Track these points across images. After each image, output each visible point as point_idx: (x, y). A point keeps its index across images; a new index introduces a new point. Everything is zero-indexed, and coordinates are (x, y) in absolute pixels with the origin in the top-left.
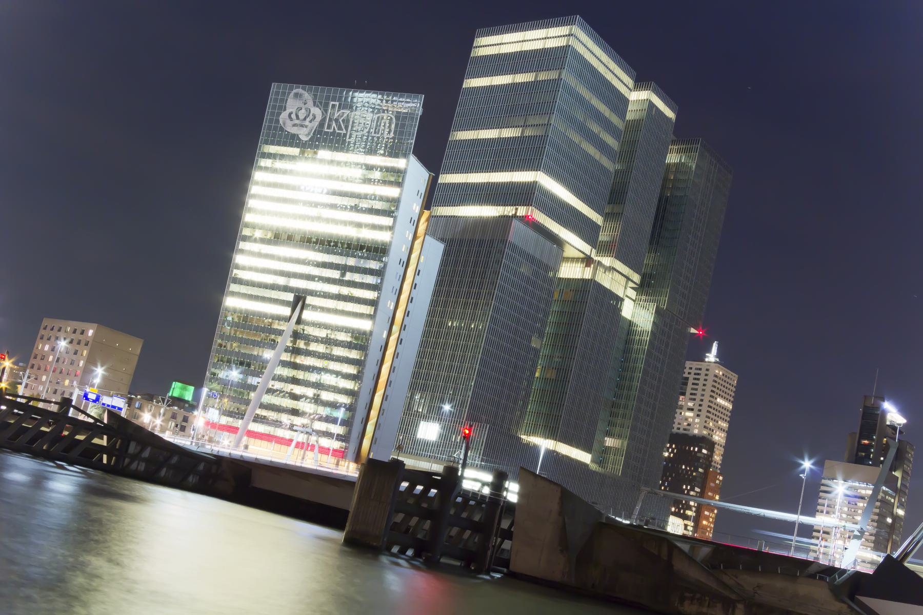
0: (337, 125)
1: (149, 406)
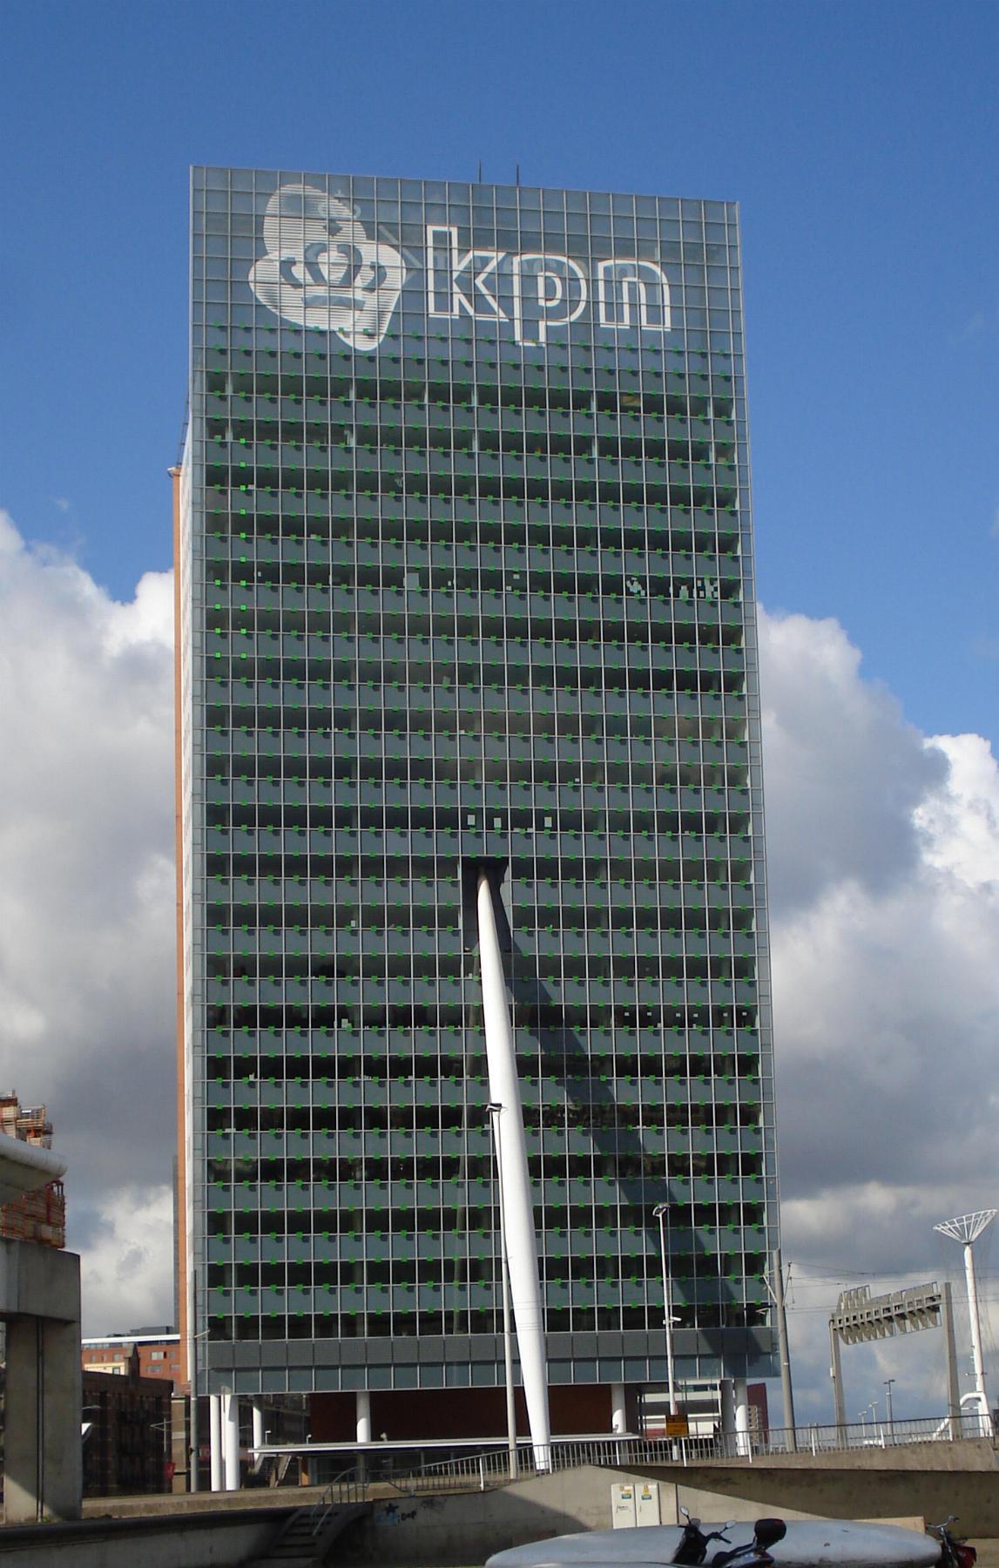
0: (468, 296)
1: (760, 1311)
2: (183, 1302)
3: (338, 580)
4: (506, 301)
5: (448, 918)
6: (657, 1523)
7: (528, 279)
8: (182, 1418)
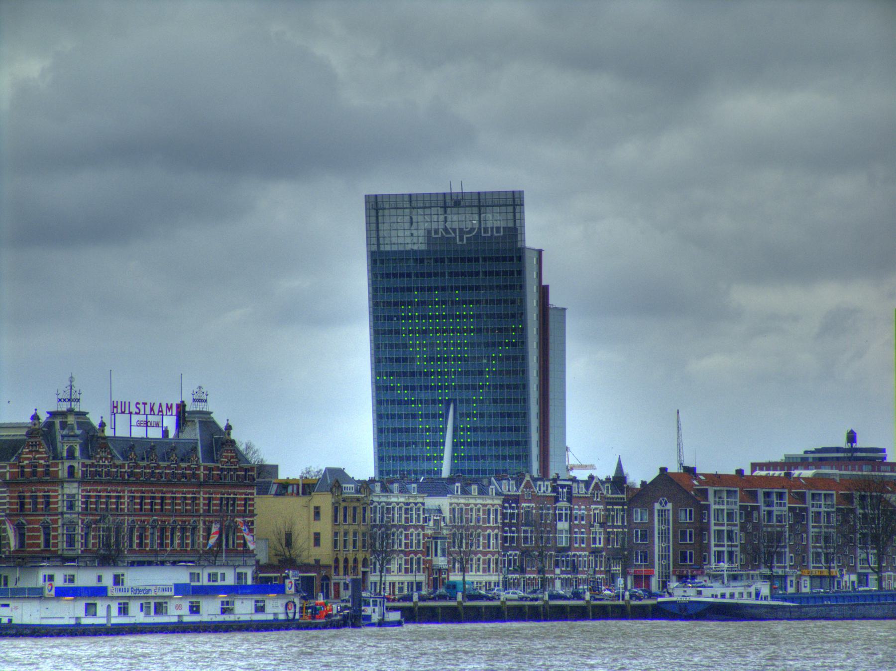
2: (873, 612)
5: (441, 416)
6: (145, 437)
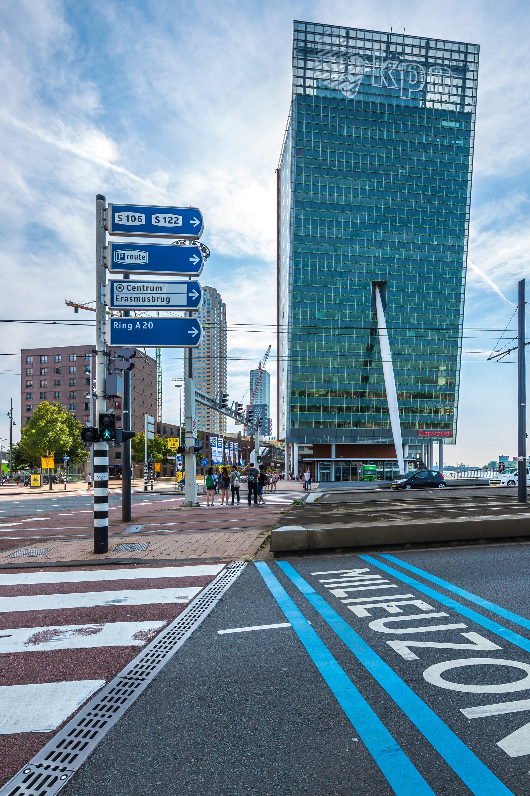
3: (316, 410)
4: (398, 80)
7: (407, 72)
8: (203, 520)
